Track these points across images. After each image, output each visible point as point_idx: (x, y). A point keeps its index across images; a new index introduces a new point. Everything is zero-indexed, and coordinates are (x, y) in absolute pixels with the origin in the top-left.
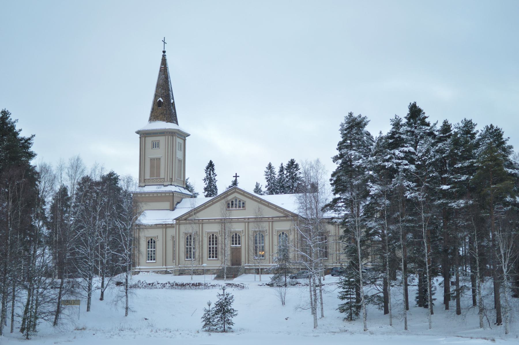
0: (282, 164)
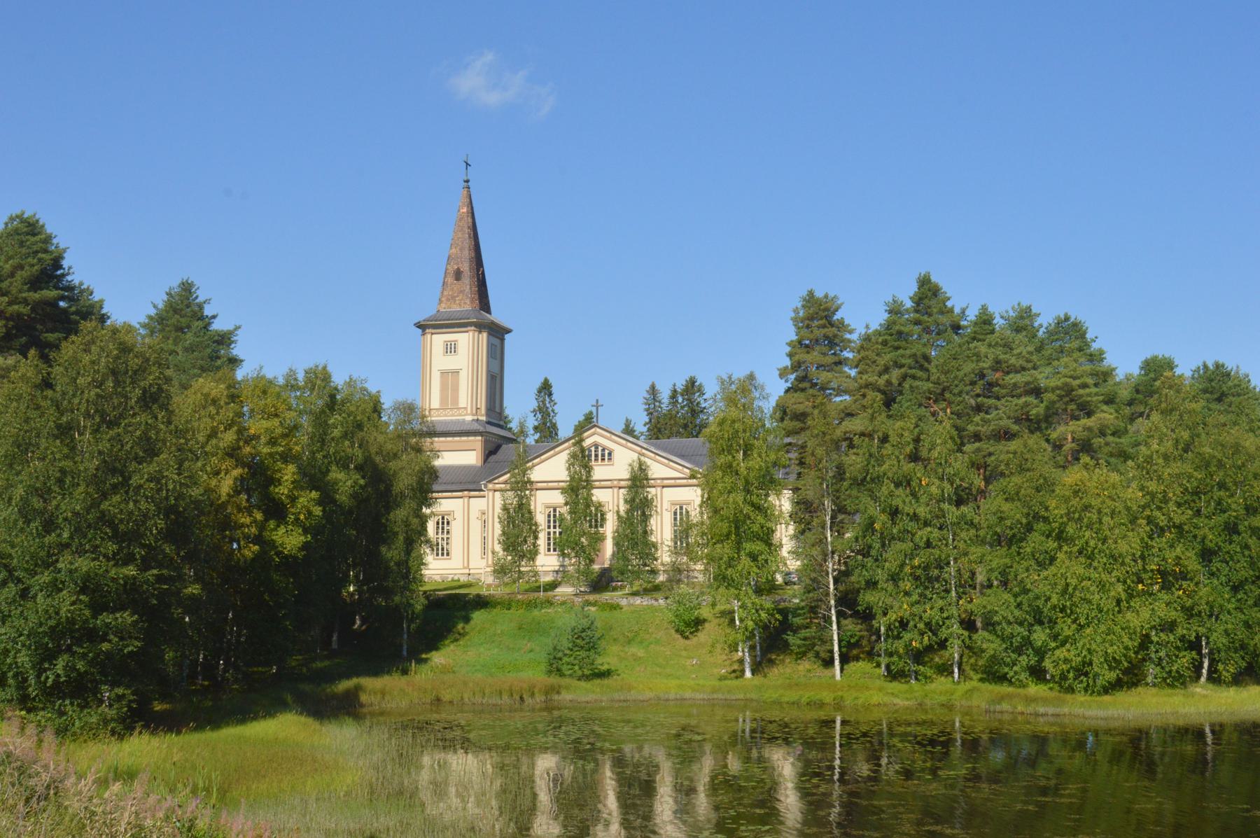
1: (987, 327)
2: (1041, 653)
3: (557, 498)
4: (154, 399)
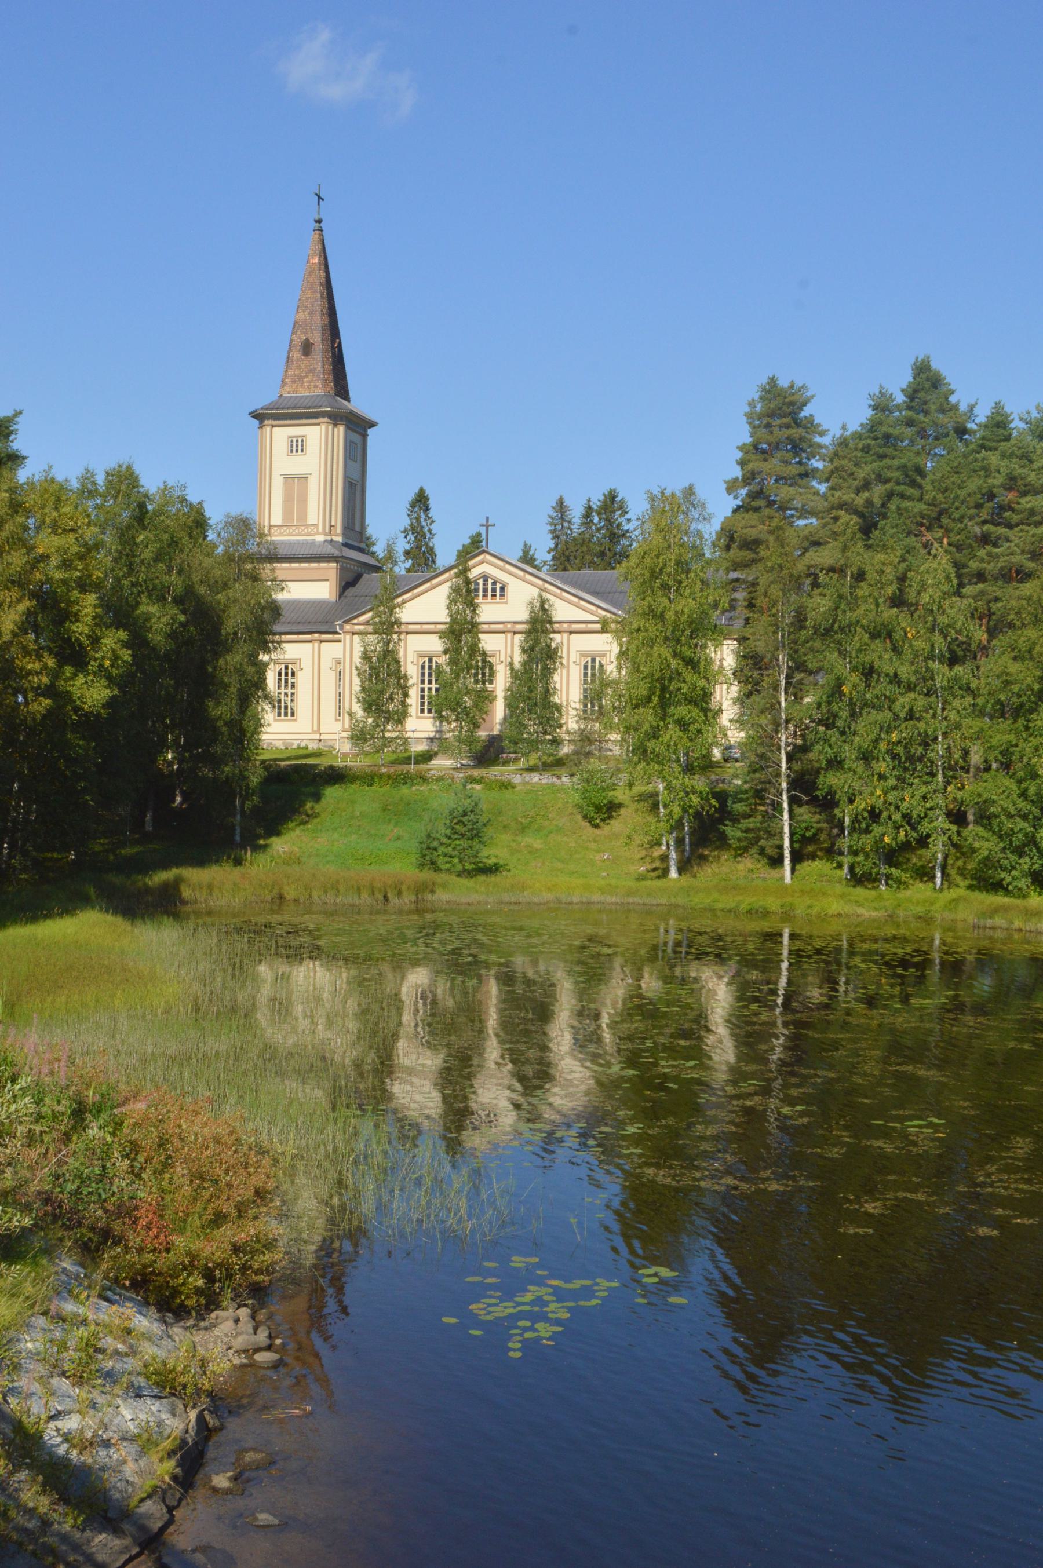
0: (589, 501)
1: (1001, 431)
3: (434, 645)
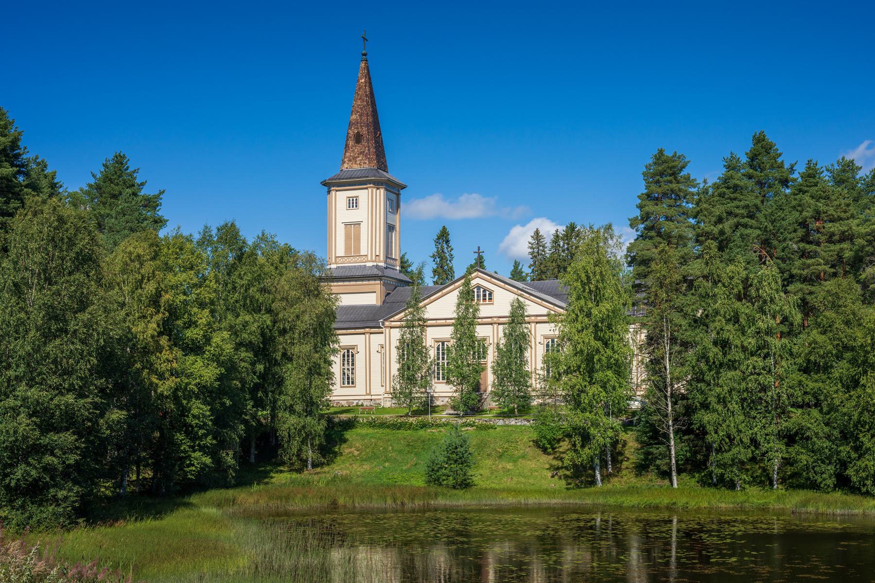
1: (812, 180)
2: (844, 464)
3: (447, 333)
4: (86, 261)
